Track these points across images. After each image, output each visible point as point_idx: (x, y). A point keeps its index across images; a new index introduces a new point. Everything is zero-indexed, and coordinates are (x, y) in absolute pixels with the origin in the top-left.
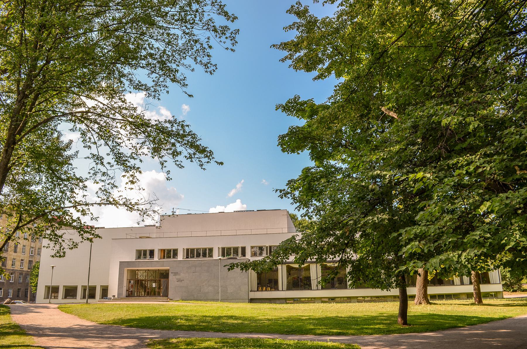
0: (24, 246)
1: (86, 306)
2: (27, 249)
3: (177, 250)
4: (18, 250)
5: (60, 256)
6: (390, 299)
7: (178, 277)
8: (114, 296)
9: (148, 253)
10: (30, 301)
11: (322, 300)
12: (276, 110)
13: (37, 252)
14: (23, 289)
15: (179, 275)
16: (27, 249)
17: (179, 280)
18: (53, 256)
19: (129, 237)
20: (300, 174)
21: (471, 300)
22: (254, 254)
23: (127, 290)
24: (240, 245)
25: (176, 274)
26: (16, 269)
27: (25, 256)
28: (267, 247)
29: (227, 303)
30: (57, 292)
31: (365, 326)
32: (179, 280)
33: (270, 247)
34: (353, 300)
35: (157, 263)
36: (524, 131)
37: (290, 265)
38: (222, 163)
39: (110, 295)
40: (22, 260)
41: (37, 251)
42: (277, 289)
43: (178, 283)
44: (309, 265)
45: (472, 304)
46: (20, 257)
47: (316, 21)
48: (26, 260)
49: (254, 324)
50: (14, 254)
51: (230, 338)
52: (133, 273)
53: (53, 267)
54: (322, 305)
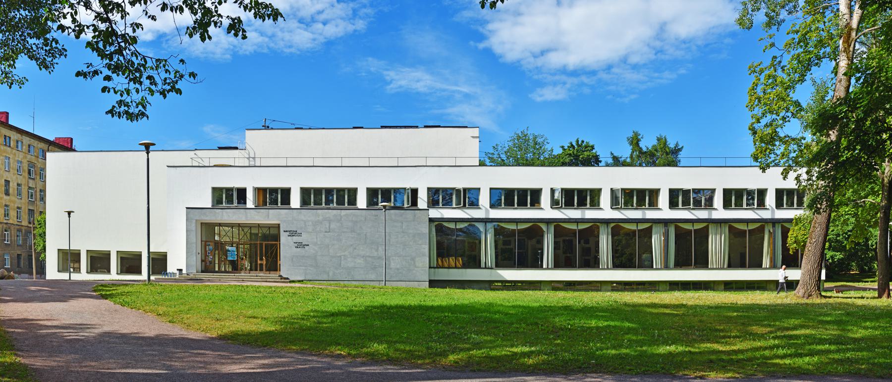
0: (19, 185)
1: (750, 64)
2: (24, 189)
3: (600, 190)
4: (11, 191)
5: (131, 117)
6: (664, 286)
7: (296, 239)
8: (180, 270)
9: (622, 201)
10: (578, 205)
11: (729, 286)
12: (784, 179)
13: (38, 196)
14: (24, 255)
15: (300, 235)
16: (24, 189)
17: (300, 245)
18: (111, 112)
19: (252, 163)
20: (632, 39)
21: (403, 83)
22: (93, 269)
23: (202, 261)
24: (409, 185)
25: (293, 233)
26: (11, 221)
27: (23, 201)
28: (458, 191)
29: (763, 302)
30: (79, 261)
31: (820, 347)
32: (300, 245)
33: (465, 190)
34: (604, 287)
35: (252, 214)
36: (229, 10)
37: (503, 225)
38: (69, 213)
39: (171, 268)
40: (18, 208)
41: (38, 194)
42: (650, 267)
43: (298, 250)
44: (707, 228)
45: (874, 298)
46: (14, 202)
47: (482, 38)
48: (25, 209)
49: (287, 51)
50: (6, 197)
51: (866, 328)
52: (208, 228)
53: (69, 213)
54: (552, 293)
